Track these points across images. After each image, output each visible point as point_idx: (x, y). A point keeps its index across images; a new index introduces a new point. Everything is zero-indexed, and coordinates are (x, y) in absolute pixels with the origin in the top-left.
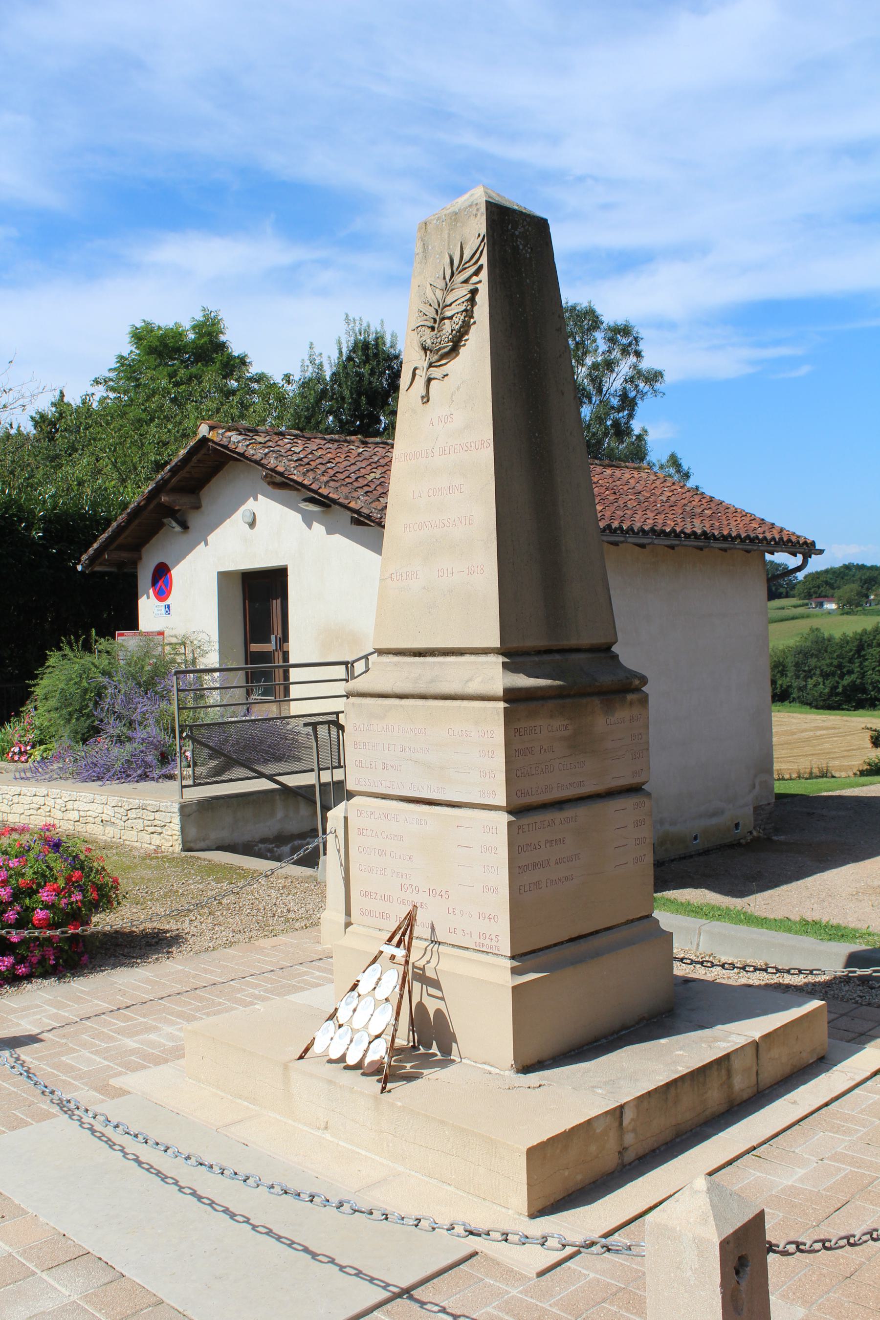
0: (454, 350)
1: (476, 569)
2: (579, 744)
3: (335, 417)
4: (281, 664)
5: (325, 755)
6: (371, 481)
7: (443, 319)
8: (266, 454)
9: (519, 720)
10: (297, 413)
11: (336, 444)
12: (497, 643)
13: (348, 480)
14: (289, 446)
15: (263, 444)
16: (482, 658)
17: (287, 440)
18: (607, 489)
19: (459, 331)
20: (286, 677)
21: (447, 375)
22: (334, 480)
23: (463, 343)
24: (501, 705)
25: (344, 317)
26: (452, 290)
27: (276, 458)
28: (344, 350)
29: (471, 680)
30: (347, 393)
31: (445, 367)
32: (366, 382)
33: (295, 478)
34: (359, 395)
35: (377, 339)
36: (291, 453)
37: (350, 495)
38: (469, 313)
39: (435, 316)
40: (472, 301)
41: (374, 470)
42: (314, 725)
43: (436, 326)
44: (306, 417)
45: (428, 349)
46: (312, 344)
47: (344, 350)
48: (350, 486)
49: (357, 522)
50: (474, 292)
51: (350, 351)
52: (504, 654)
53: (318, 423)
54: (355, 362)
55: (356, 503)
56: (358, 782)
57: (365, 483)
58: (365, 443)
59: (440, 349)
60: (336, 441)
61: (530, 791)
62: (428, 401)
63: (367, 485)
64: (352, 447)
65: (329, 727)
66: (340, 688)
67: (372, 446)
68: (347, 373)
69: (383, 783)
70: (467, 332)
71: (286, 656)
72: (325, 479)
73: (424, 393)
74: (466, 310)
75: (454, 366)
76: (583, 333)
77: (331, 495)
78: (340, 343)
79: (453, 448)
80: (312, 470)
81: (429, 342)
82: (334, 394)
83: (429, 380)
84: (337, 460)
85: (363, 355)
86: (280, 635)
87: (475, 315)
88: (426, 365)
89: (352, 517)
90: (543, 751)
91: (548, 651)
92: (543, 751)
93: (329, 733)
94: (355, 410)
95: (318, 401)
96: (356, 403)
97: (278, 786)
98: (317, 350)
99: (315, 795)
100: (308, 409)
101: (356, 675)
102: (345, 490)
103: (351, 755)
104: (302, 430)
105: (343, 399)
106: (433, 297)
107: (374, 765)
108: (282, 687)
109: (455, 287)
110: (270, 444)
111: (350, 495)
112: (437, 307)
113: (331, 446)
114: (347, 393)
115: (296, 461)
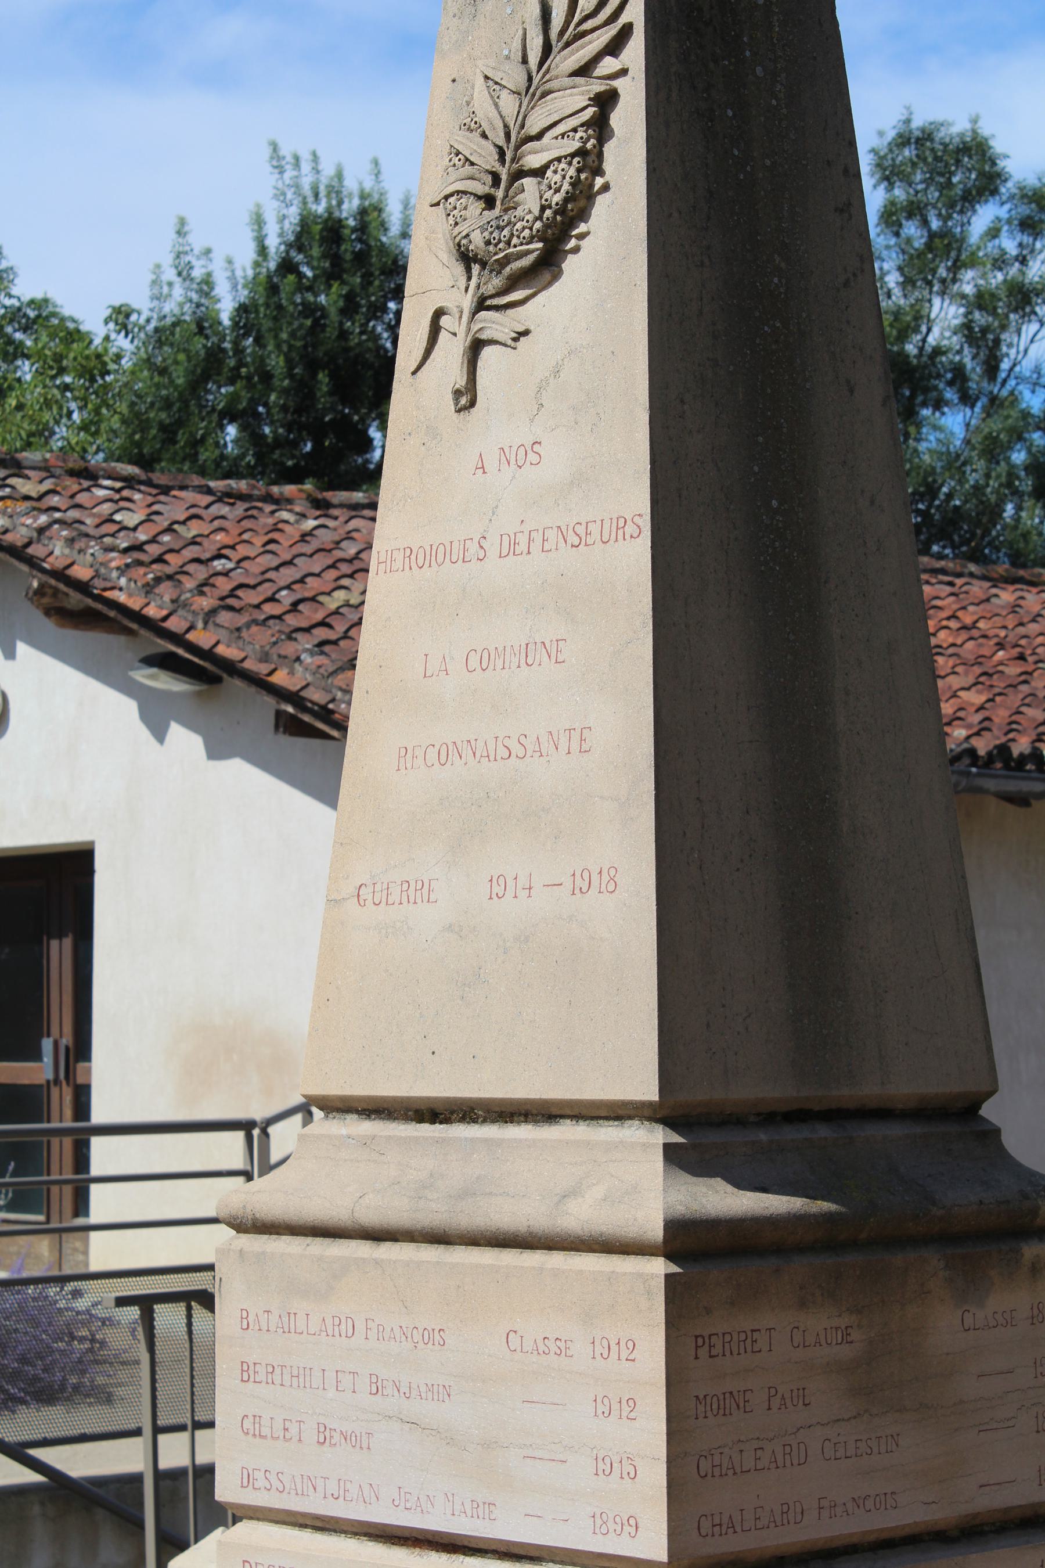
0: (548, 264)
1: (595, 877)
2: (882, 1385)
3: (242, 428)
4: (68, 1124)
5: (173, 1386)
6: (337, 612)
7: (519, 174)
8: (41, 530)
9: (708, 1311)
10: (137, 415)
11: (240, 508)
12: (648, 1091)
13: (269, 609)
14: (106, 508)
15: (36, 502)
16: (608, 1132)
17: (101, 493)
18: (1000, 646)
19: (561, 210)
20: (81, 1160)
21: (526, 333)
22: (231, 608)
23: (573, 243)
24: (658, 1267)
25: (267, 152)
26: (544, 95)
27: (70, 541)
28: (273, 242)
29: (572, 1193)
30: (276, 363)
31: (520, 309)
32: (331, 333)
33: (122, 598)
34: (313, 366)
35: (363, 212)
36: (113, 528)
37: (274, 652)
38: (590, 160)
39: (497, 167)
40: (600, 126)
41: (345, 582)
42: (146, 1303)
43: (500, 194)
44: (163, 427)
45: (475, 259)
46: (182, 222)
47: (273, 242)
48: (275, 626)
49: (290, 726)
50: (606, 101)
51: (289, 246)
52: (669, 1122)
53: (196, 443)
54: (301, 275)
55: (292, 673)
56: (248, 1480)
57: (319, 616)
58: (321, 505)
59: (507, 260)
60: (242, 497)
61: (737, 1518)
62: (472, 403)
63: (323, 624)
64: (285, 515)
65: (189, 1309)
66: (230, 1194)
67: (341, 514)
68: (280, 307)
69: (320, 1483)
70: (583, 215)
71: (82, 1106)
72: (205, 603)
73: (461, 382)
74: (582, 152)
75: (548, 308)
76: (951, 205)
77: (221, 650)
78: (259, 222)
79: (538, 537)
80: (170, 577)
81: (477, 240)
82: (241, 364)
83: (476, 346)
84: (243, 550)
85: (324, 256)
86: (67, 1040)
87: (608, 166)
88: (467, 302)
89: (279, 714)
90: (776, 1402)
91: (798, 1116)
92: (776, 1402)
93: (189, 1325)
94: (298, 411)
95: (198, 382)
96: (303, 391)
97: (36, 1478)
98: (197, 241)
99: (141, 1504)
100: (167, 404)
101: (274, 1158)
102: (261, 637)
103: (229, 1400)
104: (146, 463)
105: (267, 377)
106: (493, 113)
107: (294, 1430)
108: (68, 1190)
109: (554, 85)
110: (55, 500)
111: (274, 652)
112: (501, 141)
113: (225, 510)
114: (276, 363)
115: (126, 551)
